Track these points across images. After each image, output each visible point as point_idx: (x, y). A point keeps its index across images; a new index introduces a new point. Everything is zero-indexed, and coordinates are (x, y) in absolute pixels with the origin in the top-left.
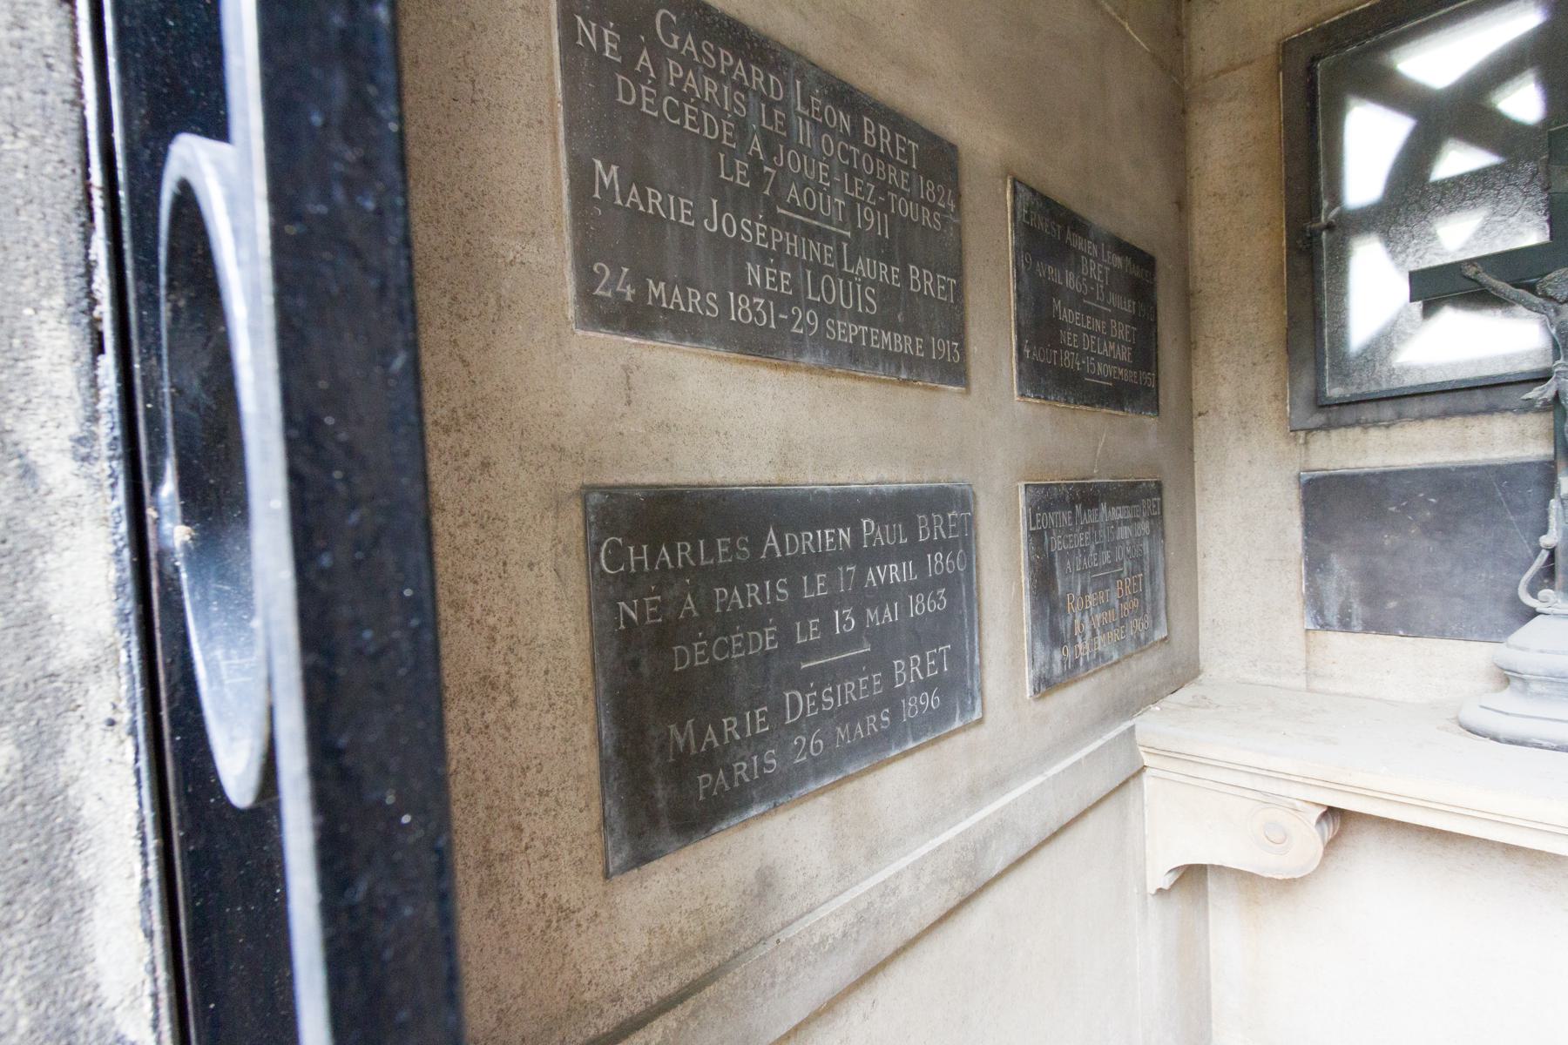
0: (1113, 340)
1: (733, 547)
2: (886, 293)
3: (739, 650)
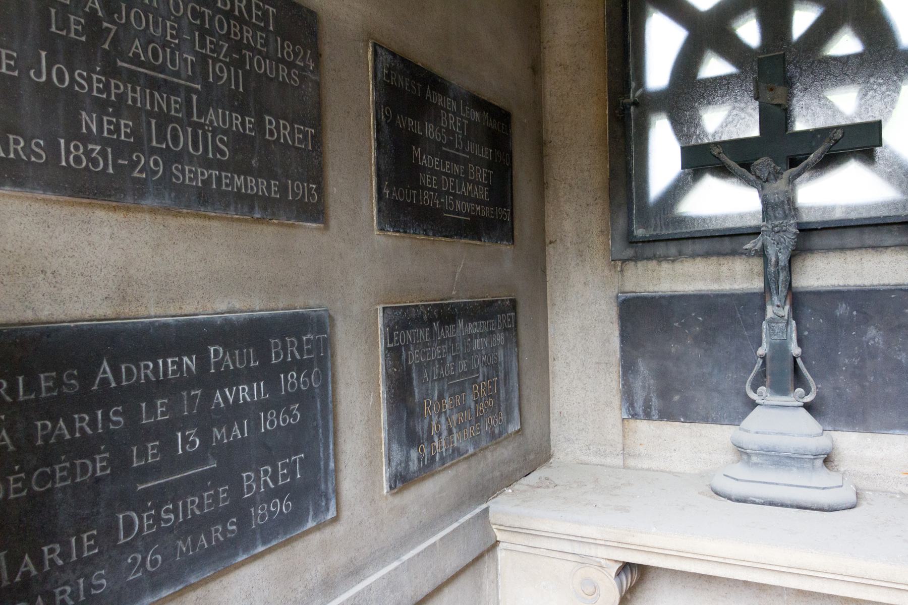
0: (470, 182)
1: (59, 383)
2: (239, 140)
3: (63, 479)
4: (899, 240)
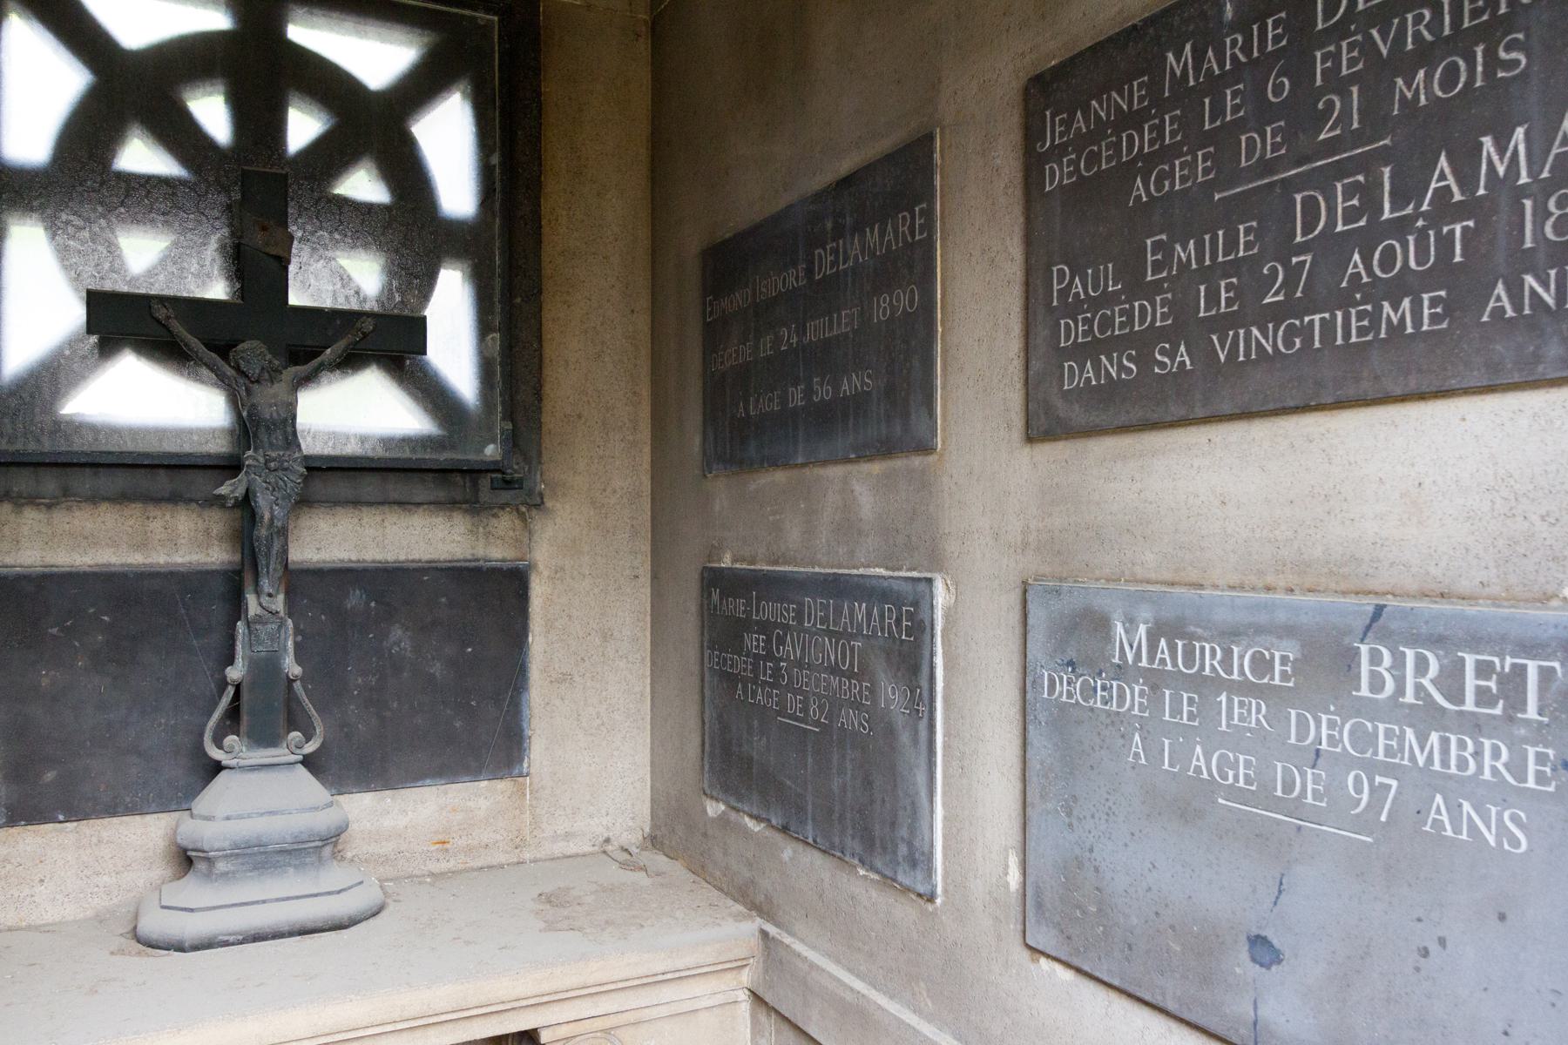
4: (441, 494)
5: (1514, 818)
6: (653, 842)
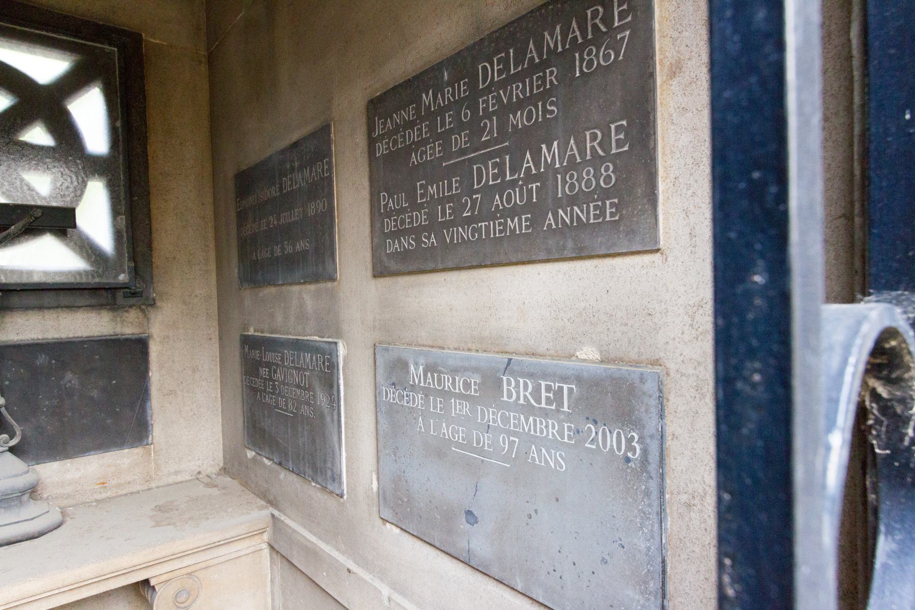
4: (94, 301)
5: (561, 456)
6: (225, 470)
